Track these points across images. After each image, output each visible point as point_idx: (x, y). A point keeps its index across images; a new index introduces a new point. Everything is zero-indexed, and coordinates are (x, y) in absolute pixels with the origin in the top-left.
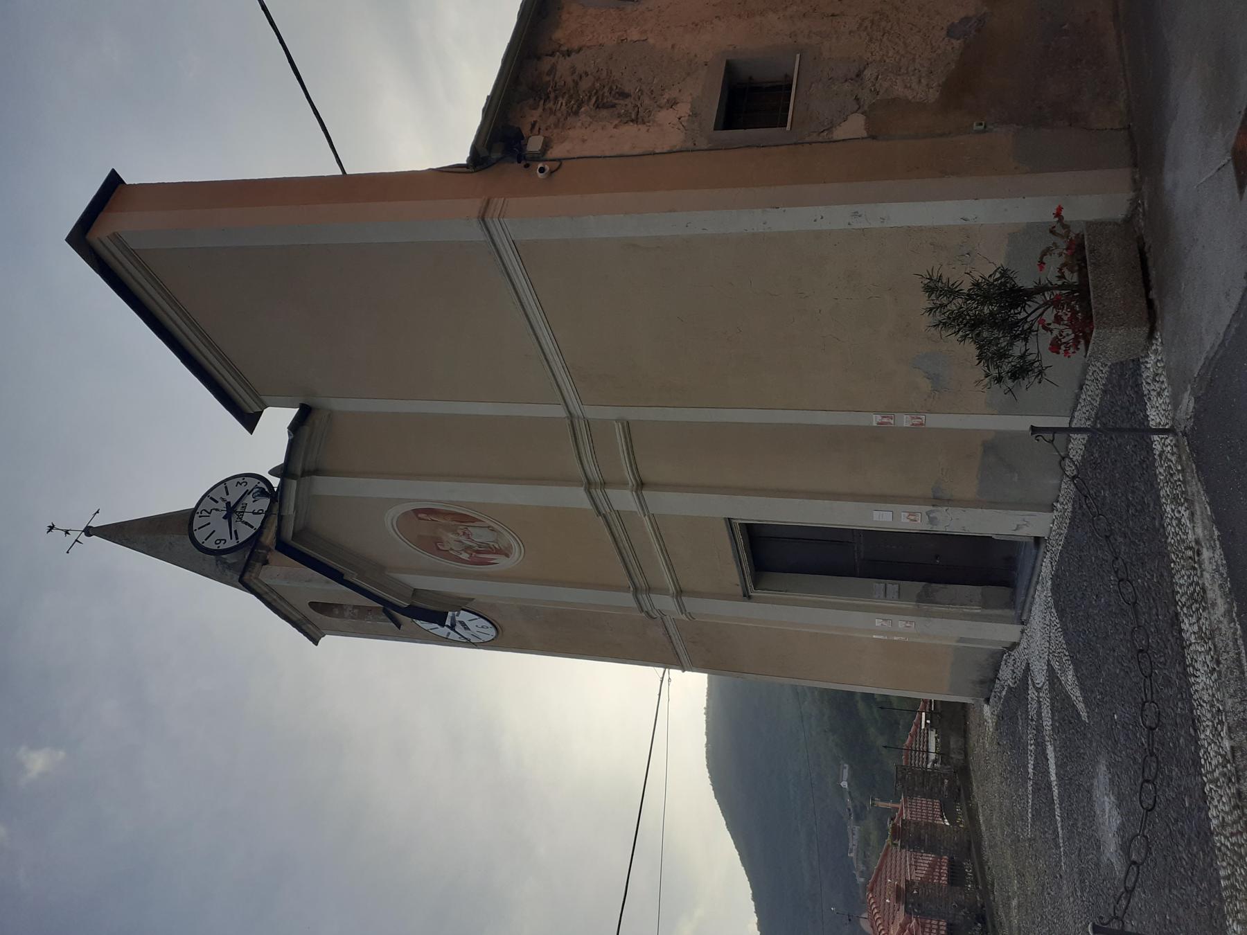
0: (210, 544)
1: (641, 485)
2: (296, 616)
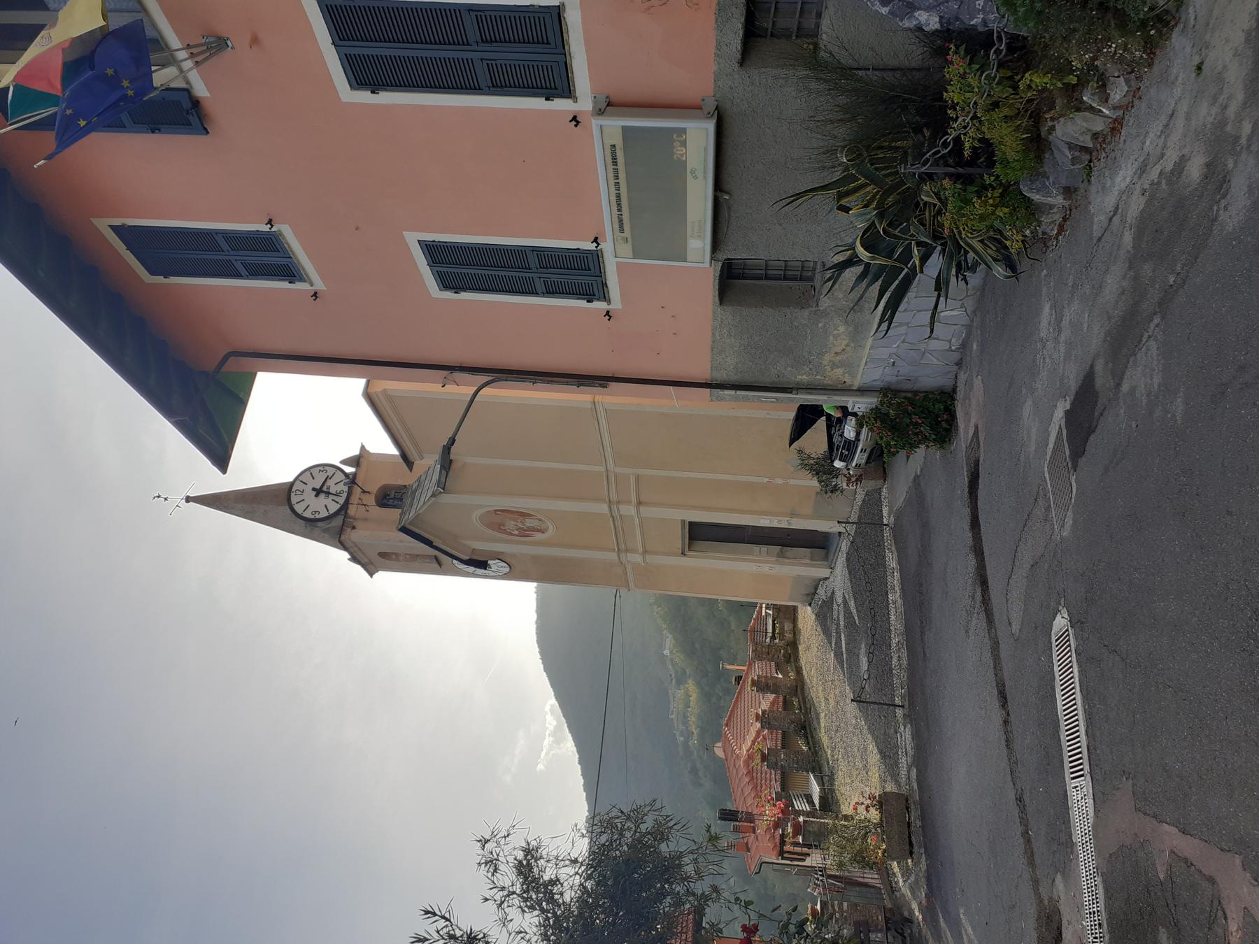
0: (308, 514)
1: (640, 503)
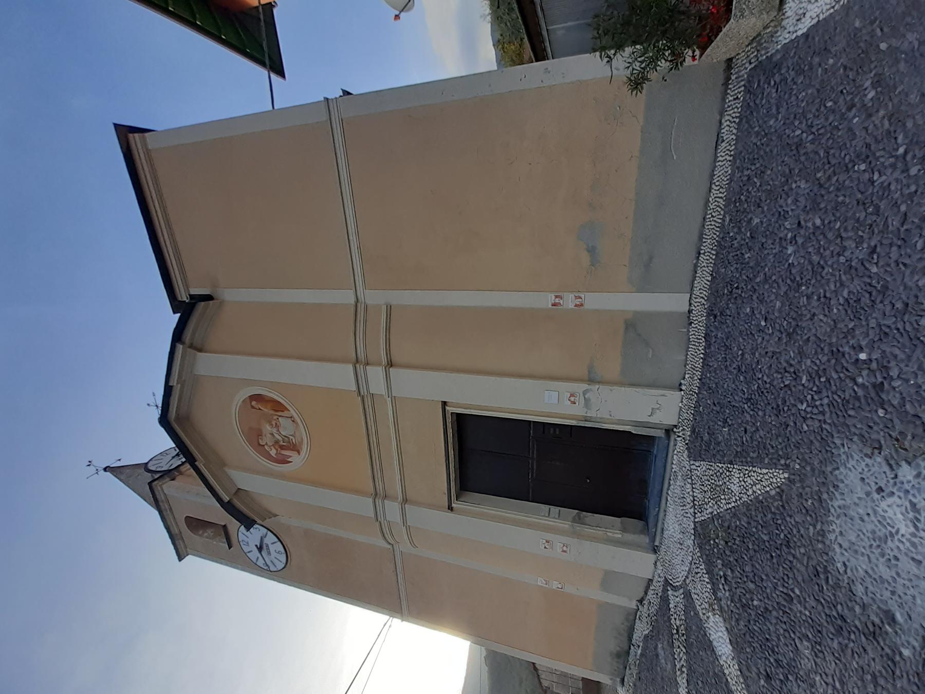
1: (391, 364)
2: (175, 530)
